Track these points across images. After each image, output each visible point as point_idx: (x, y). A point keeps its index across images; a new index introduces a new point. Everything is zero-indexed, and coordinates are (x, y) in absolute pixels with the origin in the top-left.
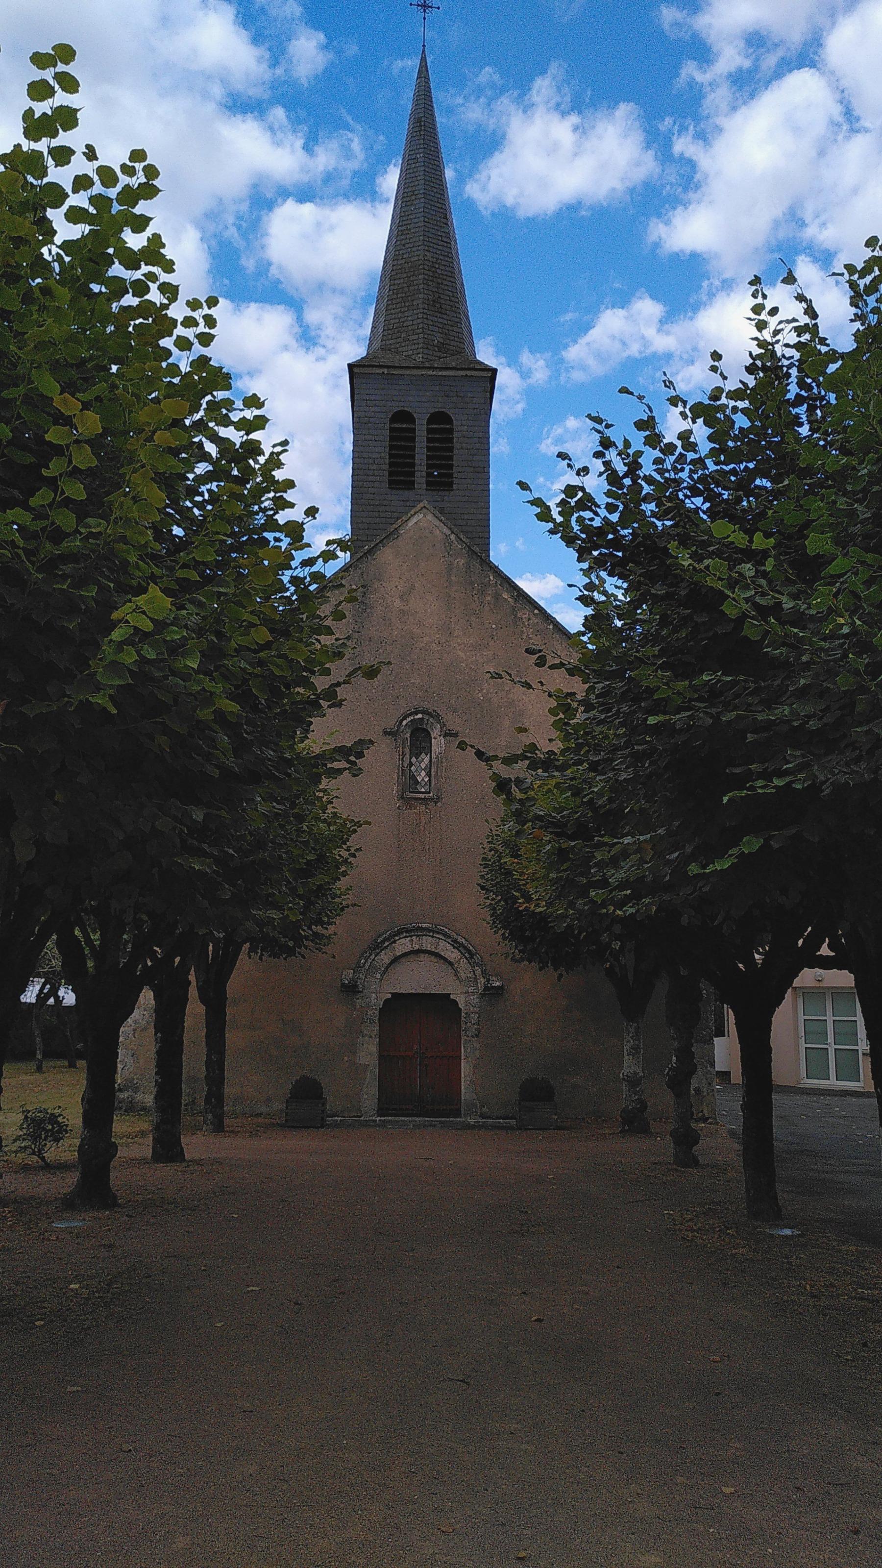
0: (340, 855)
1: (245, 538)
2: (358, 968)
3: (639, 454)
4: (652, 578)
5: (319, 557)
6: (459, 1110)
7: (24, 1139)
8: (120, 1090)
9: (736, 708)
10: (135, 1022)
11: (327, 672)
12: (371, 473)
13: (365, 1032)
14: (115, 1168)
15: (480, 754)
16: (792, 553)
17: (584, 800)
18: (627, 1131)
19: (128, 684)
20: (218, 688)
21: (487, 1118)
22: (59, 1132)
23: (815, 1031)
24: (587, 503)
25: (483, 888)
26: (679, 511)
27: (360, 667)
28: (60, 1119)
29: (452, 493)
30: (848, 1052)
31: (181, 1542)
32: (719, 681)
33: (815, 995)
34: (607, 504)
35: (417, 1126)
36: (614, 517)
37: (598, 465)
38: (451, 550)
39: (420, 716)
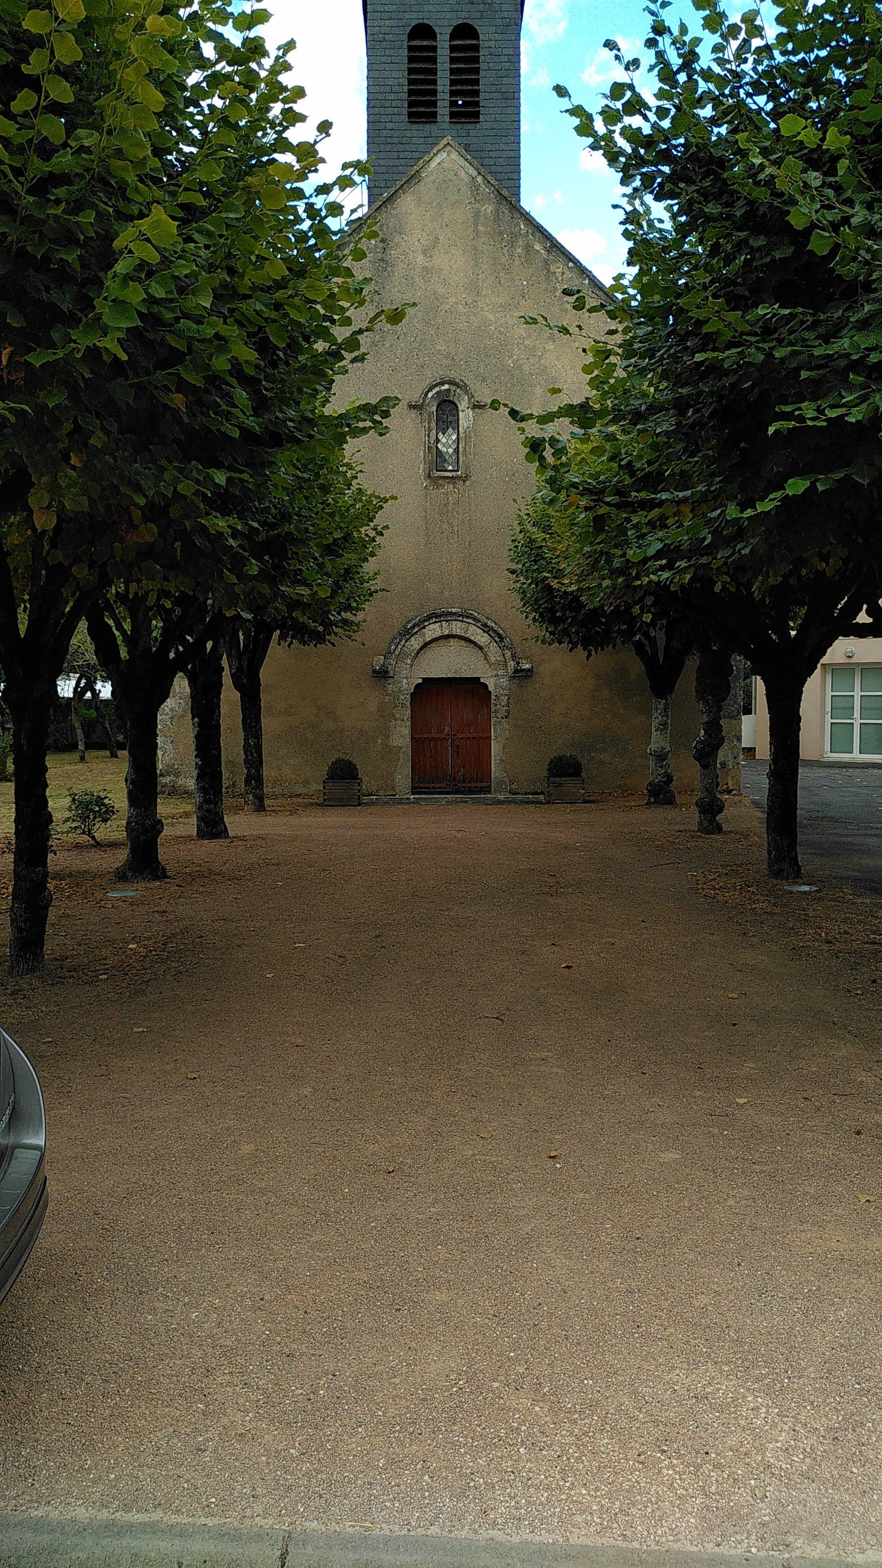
0: (367, 535)
1: (253, 162)
2: (388, 654)
3: (697, 41)
4: (706, 196)
5: (334, 184)
6: (490, 787)
7: (74, 820)
8: (162, 775)
9: (791, 344)
10: (172, 710)
11: (347, 322)
12: (388, 103)
13: (397, 716)
14: (162, 845)
15: (513, 413)
16: (865, 160)
17: (622, 463)
18: (653, 803)
19: (137, 327)
20: (231, 331)
21: (517, 794)
22: (106, 812)
23: (842, 707)
24: (636, 106)
25: (513, 572)
26: (739, 111)
27: (383, 311)
28: (106, 801)
29: (478, 126)
30: (872, 726)
31: (246, 1149)
32: (775, 315)
33: (844, 671)
34: (658, 107)
35: (448, 803)
36: (666, 124)
37: (648, 57)
38: (478, 194)
39: (446, 387)
